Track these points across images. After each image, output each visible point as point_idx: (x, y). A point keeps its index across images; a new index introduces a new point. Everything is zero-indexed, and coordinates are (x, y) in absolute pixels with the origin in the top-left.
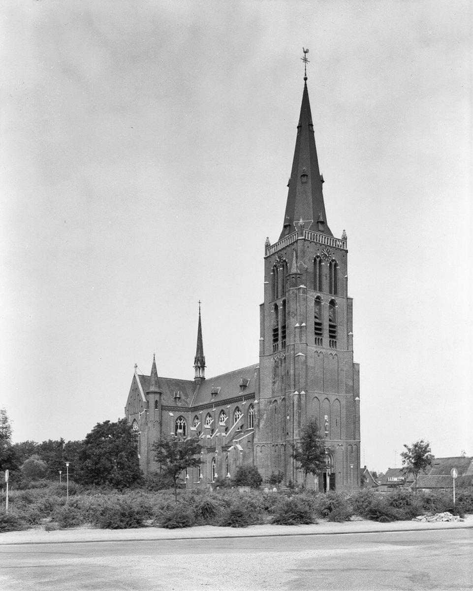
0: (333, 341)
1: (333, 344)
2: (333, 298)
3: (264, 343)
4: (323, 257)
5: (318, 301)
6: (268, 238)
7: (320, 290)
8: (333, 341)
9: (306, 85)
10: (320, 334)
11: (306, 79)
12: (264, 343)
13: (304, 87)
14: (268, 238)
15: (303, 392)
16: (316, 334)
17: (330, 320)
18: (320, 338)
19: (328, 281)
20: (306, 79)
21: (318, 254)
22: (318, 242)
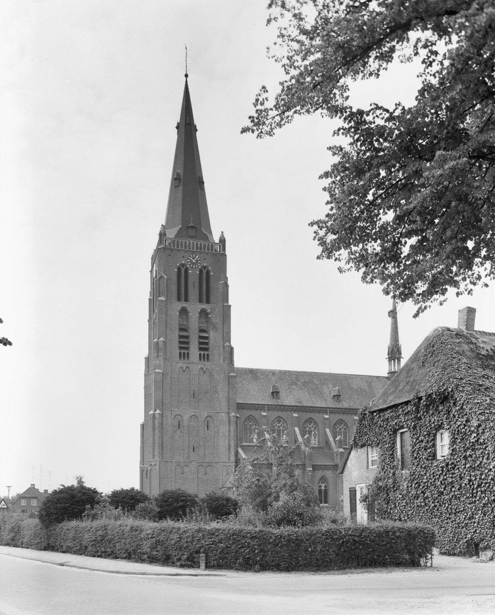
0: (184, 353)
1: (204, 358)
2: (184, 305)
3: (148, 361)
4: (190, 265)
5: (184, 311)
6: (222, 232)
7: (186, 300)
8: (204, 354)
9: (186, 82)
10: (207, 349)
11: (186, 76)
12: (148, 361)
13: (184, 87)
14: (222, 232)
15: (162, 339)
16: (201, 349)
17: (181, 330)
18: (206, 353)
19: (197, 292)
20: (186, 76)
21: (183, 262)
22: (180, 248)
